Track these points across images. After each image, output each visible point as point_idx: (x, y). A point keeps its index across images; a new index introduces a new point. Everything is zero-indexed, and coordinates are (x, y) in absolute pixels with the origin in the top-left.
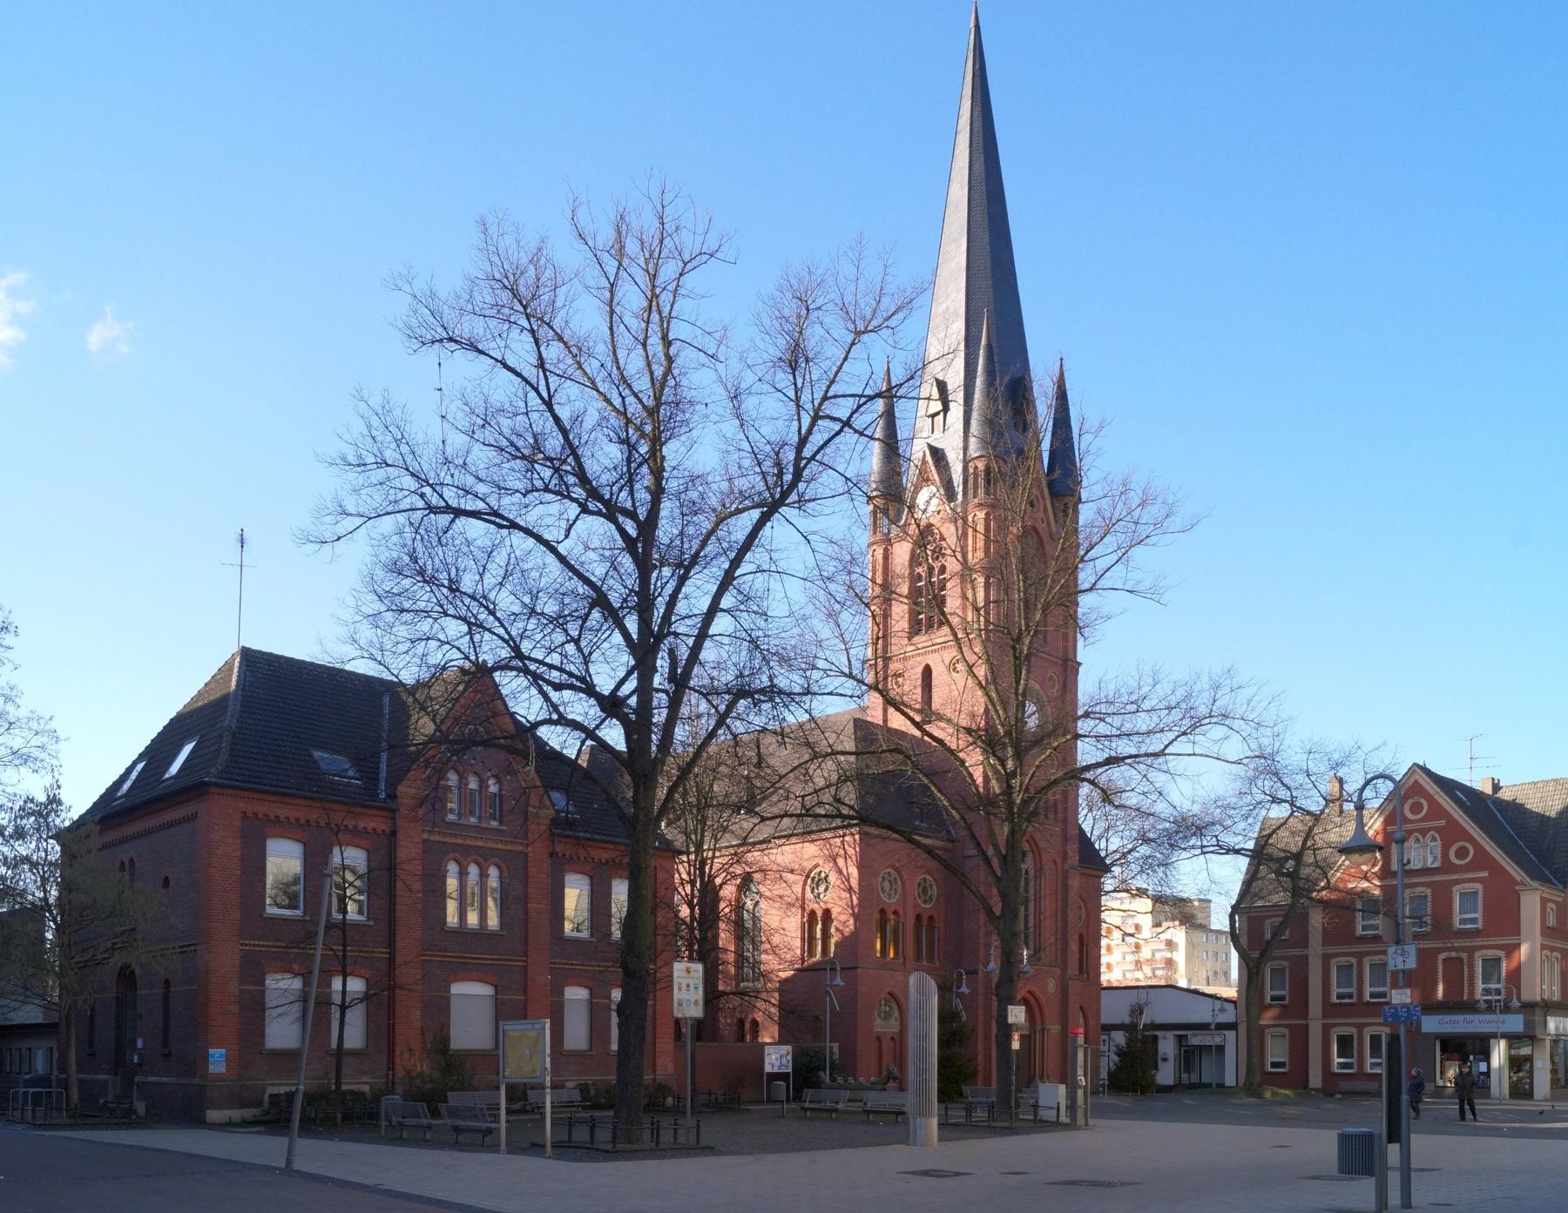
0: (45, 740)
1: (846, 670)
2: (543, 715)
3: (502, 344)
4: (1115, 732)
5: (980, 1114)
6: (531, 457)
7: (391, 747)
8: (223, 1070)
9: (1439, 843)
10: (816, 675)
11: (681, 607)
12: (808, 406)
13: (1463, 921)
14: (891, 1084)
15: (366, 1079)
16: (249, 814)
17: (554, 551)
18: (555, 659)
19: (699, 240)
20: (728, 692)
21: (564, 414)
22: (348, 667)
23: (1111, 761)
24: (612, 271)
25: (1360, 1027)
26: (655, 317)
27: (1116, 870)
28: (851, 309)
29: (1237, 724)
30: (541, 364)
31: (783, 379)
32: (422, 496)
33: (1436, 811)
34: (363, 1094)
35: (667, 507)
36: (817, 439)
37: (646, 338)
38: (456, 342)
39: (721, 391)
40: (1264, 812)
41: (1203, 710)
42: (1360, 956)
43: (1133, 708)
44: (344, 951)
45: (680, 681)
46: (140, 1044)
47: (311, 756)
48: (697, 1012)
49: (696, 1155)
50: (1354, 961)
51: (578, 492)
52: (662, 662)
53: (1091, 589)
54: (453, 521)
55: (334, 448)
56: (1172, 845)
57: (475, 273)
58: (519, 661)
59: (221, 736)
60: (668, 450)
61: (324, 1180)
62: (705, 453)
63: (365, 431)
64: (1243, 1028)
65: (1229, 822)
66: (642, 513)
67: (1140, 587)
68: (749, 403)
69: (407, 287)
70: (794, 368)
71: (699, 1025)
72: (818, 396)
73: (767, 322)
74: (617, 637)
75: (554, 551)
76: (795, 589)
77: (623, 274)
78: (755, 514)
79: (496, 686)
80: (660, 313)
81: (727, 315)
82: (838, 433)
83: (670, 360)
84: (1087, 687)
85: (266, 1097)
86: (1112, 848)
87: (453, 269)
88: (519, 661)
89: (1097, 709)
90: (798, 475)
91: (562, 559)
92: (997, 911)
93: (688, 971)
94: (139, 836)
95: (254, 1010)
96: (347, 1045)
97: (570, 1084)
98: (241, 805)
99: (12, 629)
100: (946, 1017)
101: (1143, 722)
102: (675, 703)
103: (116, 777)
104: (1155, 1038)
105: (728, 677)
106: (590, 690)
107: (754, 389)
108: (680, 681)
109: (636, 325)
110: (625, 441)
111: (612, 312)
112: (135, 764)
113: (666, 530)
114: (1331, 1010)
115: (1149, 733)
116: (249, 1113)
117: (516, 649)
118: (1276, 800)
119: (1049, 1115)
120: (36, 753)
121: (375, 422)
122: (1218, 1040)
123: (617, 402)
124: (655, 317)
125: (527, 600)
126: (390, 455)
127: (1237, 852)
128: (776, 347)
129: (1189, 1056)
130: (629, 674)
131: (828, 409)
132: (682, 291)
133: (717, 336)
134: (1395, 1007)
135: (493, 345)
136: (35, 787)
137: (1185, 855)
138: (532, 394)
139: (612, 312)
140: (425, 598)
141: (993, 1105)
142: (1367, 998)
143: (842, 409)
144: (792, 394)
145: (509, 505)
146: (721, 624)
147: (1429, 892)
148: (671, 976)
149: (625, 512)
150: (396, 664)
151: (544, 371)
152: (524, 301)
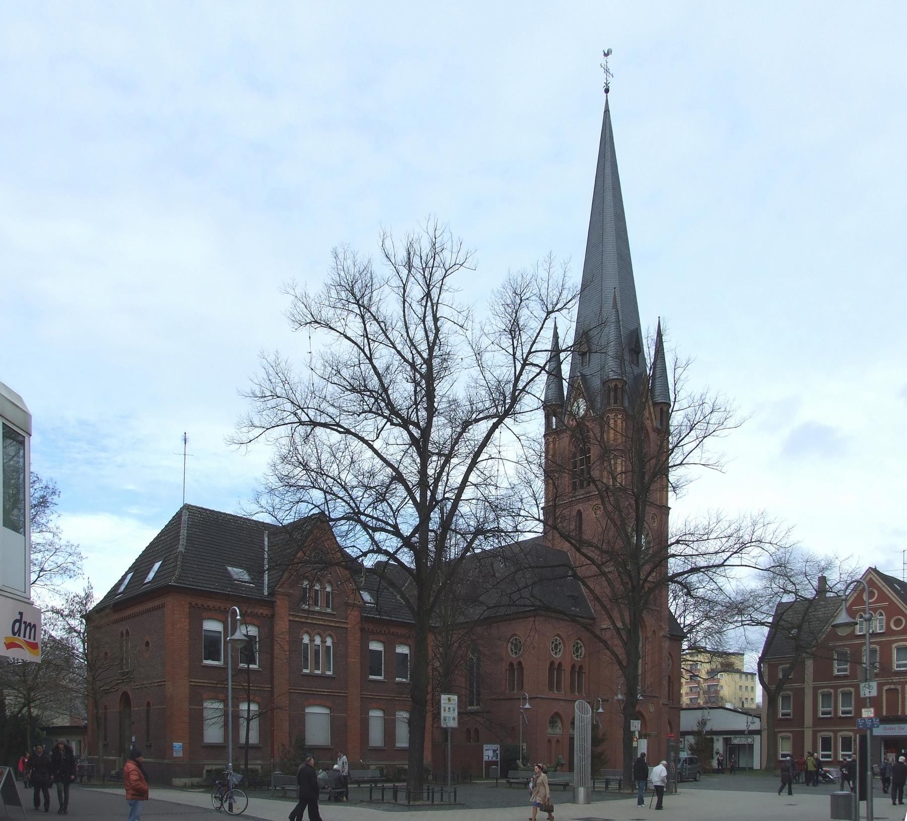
0: (75, 558)
4: (695, 553)
5: (614, 786)
6: (359, 389)
8: (181, 755)
9: (884, 617)
12: (520, 358)
13: (898, 666)
15: (259, 762)
16: (193, 604)
17: (371, 447)
19: (454, 256)
22: (254, 518)
23: (695, 570)
24: (404, 277)
25: (836, 732)
26: (429, 304)
28: (545, 299)
29: (767, 546)
30: (366, 335)
31: (506, 342)
32: (296, 414)
33: (883, 597)
34: (257, 770)
35: (438, 421)
36: (524, 378)
38: (319, 323)
40: (779, 599)
41: (747, 538)
42: (836, 688)
43: (705, 537)
44: (249, 686)
46: (134, 739)
47: (226, 569)
49: (443, 809)
50: (832, 691)
51: (387, 413)
52: (435, 516)
53: (681, 464)
56: (723, 620)
57: (330, 282)
58: (355, 516)
59: (177, 557)
60: (441, 388)
62: (459, 386)
63: (265, 377)
64: (765, 733)
65: (758, 605)
67: (710, 462)
68: (486, 357)
69: (292, 292)
72: (526, 351)
75: (371, 447)
77: (412, 279)
80: (431, 300)
82: (538, 374)
83: (437, 330)
84: (676, 523)
85: (204, 771)
86: (687, 622)
87: (317, 283)
88: (355, 516)
89: (683, 538)
91: (375, 451)
93: (449, 700)
94: (128, 618)
95: (197, 722)
99: (57, 493)
101: (712, 546)
104: (712, 740)
106: (396, 532)
107: (489, 349)
108: (446, 524)
109: (420, 310)
110: (414, 381)
112: (127, 573)
114: (818, 722)
116: (196, 780)
118: (786, 592)
120: (71, 566)
121: (271, 371)
122: (750, 740)
126: (279, 391)
127: (763, 624)
128: (501, 324)
129: (732, 750)
131: (532, 359)
132: (444, 287)
133: (465, 313)
134: (864, 719)
136: (76, 587)
137: (732, 626)
138: (362, 354)
139: (404, 301)
140: (304, 478)
141: (620, 781)
142: (840, 714)
146: (468, 493)
147: (878, 647)
148: (440, 700)
149: (413, 424)
150: (280, 515)
151: (368, 339)
152: (357, 295)
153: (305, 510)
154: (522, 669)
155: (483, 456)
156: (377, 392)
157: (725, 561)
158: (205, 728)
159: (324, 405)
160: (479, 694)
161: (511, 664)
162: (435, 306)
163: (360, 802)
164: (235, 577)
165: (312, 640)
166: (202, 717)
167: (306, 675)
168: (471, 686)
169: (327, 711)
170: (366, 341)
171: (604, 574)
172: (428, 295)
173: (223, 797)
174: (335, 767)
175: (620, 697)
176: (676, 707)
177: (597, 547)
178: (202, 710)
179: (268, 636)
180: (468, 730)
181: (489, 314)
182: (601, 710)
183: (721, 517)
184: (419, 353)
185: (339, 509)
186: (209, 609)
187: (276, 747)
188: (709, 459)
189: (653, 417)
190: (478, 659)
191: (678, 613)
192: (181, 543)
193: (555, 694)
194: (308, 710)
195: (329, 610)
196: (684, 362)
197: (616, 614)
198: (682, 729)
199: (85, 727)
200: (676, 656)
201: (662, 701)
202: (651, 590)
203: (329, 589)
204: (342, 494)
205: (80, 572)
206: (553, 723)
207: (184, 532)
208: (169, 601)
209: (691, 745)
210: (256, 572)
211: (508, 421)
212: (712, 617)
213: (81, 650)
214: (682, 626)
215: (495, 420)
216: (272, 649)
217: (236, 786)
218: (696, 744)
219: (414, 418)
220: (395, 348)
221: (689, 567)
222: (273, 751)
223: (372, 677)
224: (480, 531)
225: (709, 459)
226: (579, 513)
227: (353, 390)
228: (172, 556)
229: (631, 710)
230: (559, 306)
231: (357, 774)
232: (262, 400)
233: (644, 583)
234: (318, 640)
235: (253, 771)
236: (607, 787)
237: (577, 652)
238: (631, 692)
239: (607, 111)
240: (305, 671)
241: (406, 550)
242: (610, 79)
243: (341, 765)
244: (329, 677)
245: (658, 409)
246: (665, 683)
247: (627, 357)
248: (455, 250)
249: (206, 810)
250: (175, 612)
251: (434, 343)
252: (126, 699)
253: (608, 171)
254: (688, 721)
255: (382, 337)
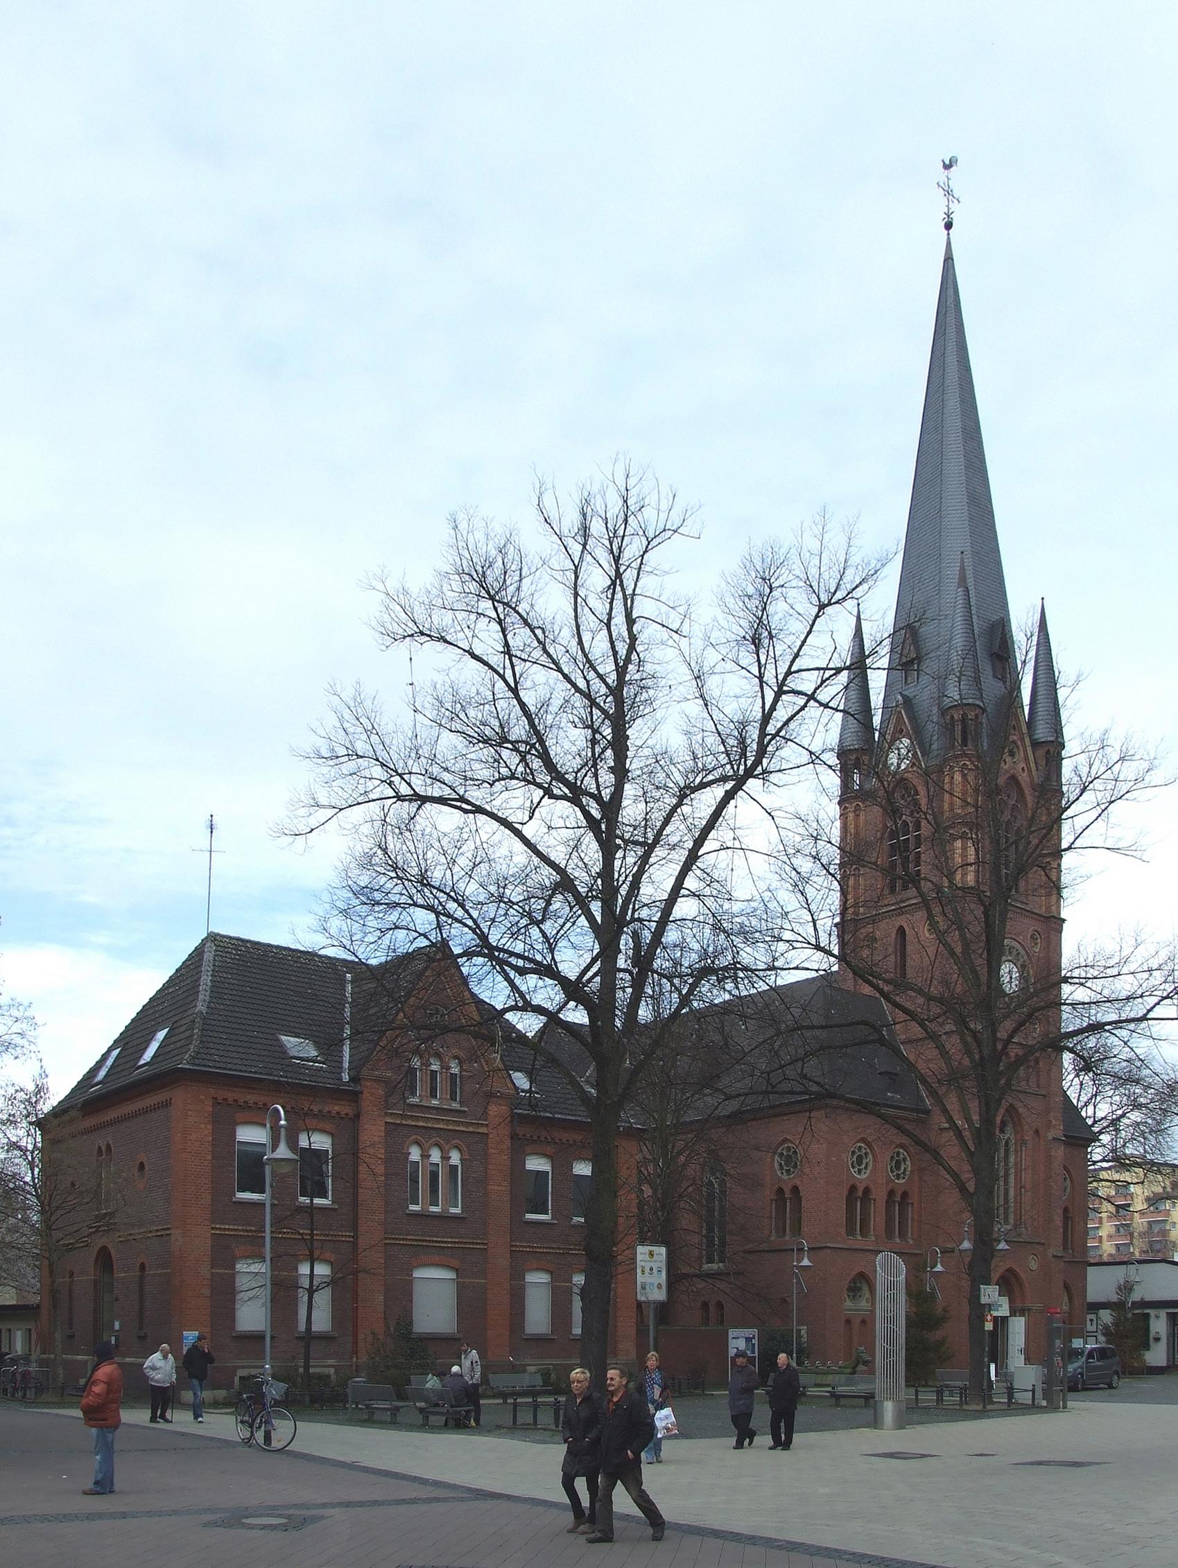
1: (813, 941)
2: (511, 1003)
3: (470, 635)
5: (951, 1399)
7: (355, 1033)
10: (782, 946)
11: (646, 890)
12: (772, 682)
14: (861, 1367)
15: (331, 1362)
17: (518, 834)
18: (519, 947)
19: (663, 516)
20: (691, 975)
21: (528, 698)
22: (322, 952)
26: (619, 595)
27: (1105, 1138)
28: (815, 584)
31: (748, 659)
34: (329, 1376)
35: (629, 790)
36: (781, 714)
37: (610, 619)
39: (684, 669)
45: (643, 961)
46: (117, 1326)
47: (279, 1040)
48: (660, 1295)
51: (543, 778)
52: (626, 942)
53: (1070, 848)
54: (420, 807)
55: (309, 742)
57: (447, 568)
60: (637, 733)
61: (323, 1460)
62: (668, 730)
63: (338, 725)
66: (606, 794)
68: (712, 683)
69: (380, 587)
70: (756, 642)
71: (664, 1311)
72: (782, 670)
73: (731, 601)
74: (583, 921)
75: (518, 834)
76: (759, 864)
77: (588, 558)
78: (719, 791)
79: (465, 980)
80: (623, 590)
81: (691, 590)
82: (802, 708)
83: (633, 638)
85: (237, 1379)
86: (1100, 1114)
87: (425, 569)
88: (485, 948)
89: (1076, 973)
90: (762, 752)
92: (971, 1187)
93: (651, 1254)
95: (224, 1296)
96: (315, 1328)
97: (532, 1369)
98: (212, 1091)
100: (918, 1296)
101: (1125, 986)
102: (638, 985)
103: (92, 1064)
105: (690, 959)
108: (643, 961)
111: (576, 595)
112: (110, 1050)
113: (631, 810)
115: (1128, 998)
116: (221, 1394)
117: (484, 938)
119: (1026, 1398)
120: (17, 1040)
123: (581, 684)
124: (619, 595)
125: (493, 889)
126: (361, 747)
128: (741, 627)
130: (594, 961)
131: (792, 683)
133: (682, 610)
135: (461, 635)
139: (576, 595)
143: (807, 683)
144: (755, 671)
145: (476, 795)
148: (634, 1259)
151: (511, 656)
152: (492, 588)
153: (403, 942)
154: (800, 1199)
155: (708, 846)
156: (527, 743)
157: (1149, 1011)
158: (237, 1306)
159: (435, 770)
160: (723, 1243)
161: (780, 1191)
162: (629, 601)
163: (496, 1429)
164: (293, 1053)
165: (426, 1156)
166: (233, 1287)
167: (415, 1215)
168: (711, 1230)
169: (450, 1275)
170: (507, 661)
171: (933, 1037)
172: (617, 579)
173: (253, 1421)
174: (455, 1369)
175: (966, 1245)
176: (1077, 1258)
177: (920, 992)
178: (233, 1276)
179: (349, 1150)
180: (705, 1305)
181: (717, 612)
182: (939, 1268)
183: (1143, 937)
184: (600, 676)
185: (460, 939)
186: (246, 1107)
187: (361, 1337)
188: (1120, 839)
189: (1033, 765)
190: (722, 1183)
191: (1084, 1099)
192: (201, 997)
193: (858, 1241)
194: (418, 1273)
195: (455, 1105)
196: (1073, 678)
197: (952, 1103)
198: (1091, 1297)
199: (38, 1306)
200: (1078, 1175)
201: (1052, 1251)
202: (1020, 1061)
203: (455, 1070)
204: (460, 913)
205: (33, 1048)
206: (854, 1290)
207: (206, 980)
208: (179, 1096)
209: (1106, 1327)
210: (329, 1047)
211: (752, 785)
212: (1145, 1106)
213: (28, 1179)
214: (1090, 1122)
215: (729, 785)
216: (356, 1172)
217: (277, 1403)
218: (1116, 1324)
219: (589, 784)
220: (560, 670)
221: (1085, 1024)
222: (355, 1343)
223: (530, 1216)
224: (702, 973)
225: (1120, 839)
226: (901, 931)
227: (486, 741)
228: (183, 1022)
229: (979, 1268)
230: (839, 595)
231: (501, 1381)
232: (331, 763)
233: (1005, 1047)
234: (435, 1156)
235: (320, 1377)
236: (940, 1400)
237: (898, 1168)
238: (984, 1240)
239: (949, 259)
240: (413, 1208)
241: (572, 1004)
242: (953, 207)
243: (467, 1366)
244: (455, 1218)
245: (1041, 752)
246: (1058, 1220)
247: (986, 667)
248: (664, 506)
249: (227, 1443)
250: (189, 1112)
251: (628, 660)
252: (105, 1260)
253: (951, 359)
254: (1101, 1285)
255: (538, 653)
